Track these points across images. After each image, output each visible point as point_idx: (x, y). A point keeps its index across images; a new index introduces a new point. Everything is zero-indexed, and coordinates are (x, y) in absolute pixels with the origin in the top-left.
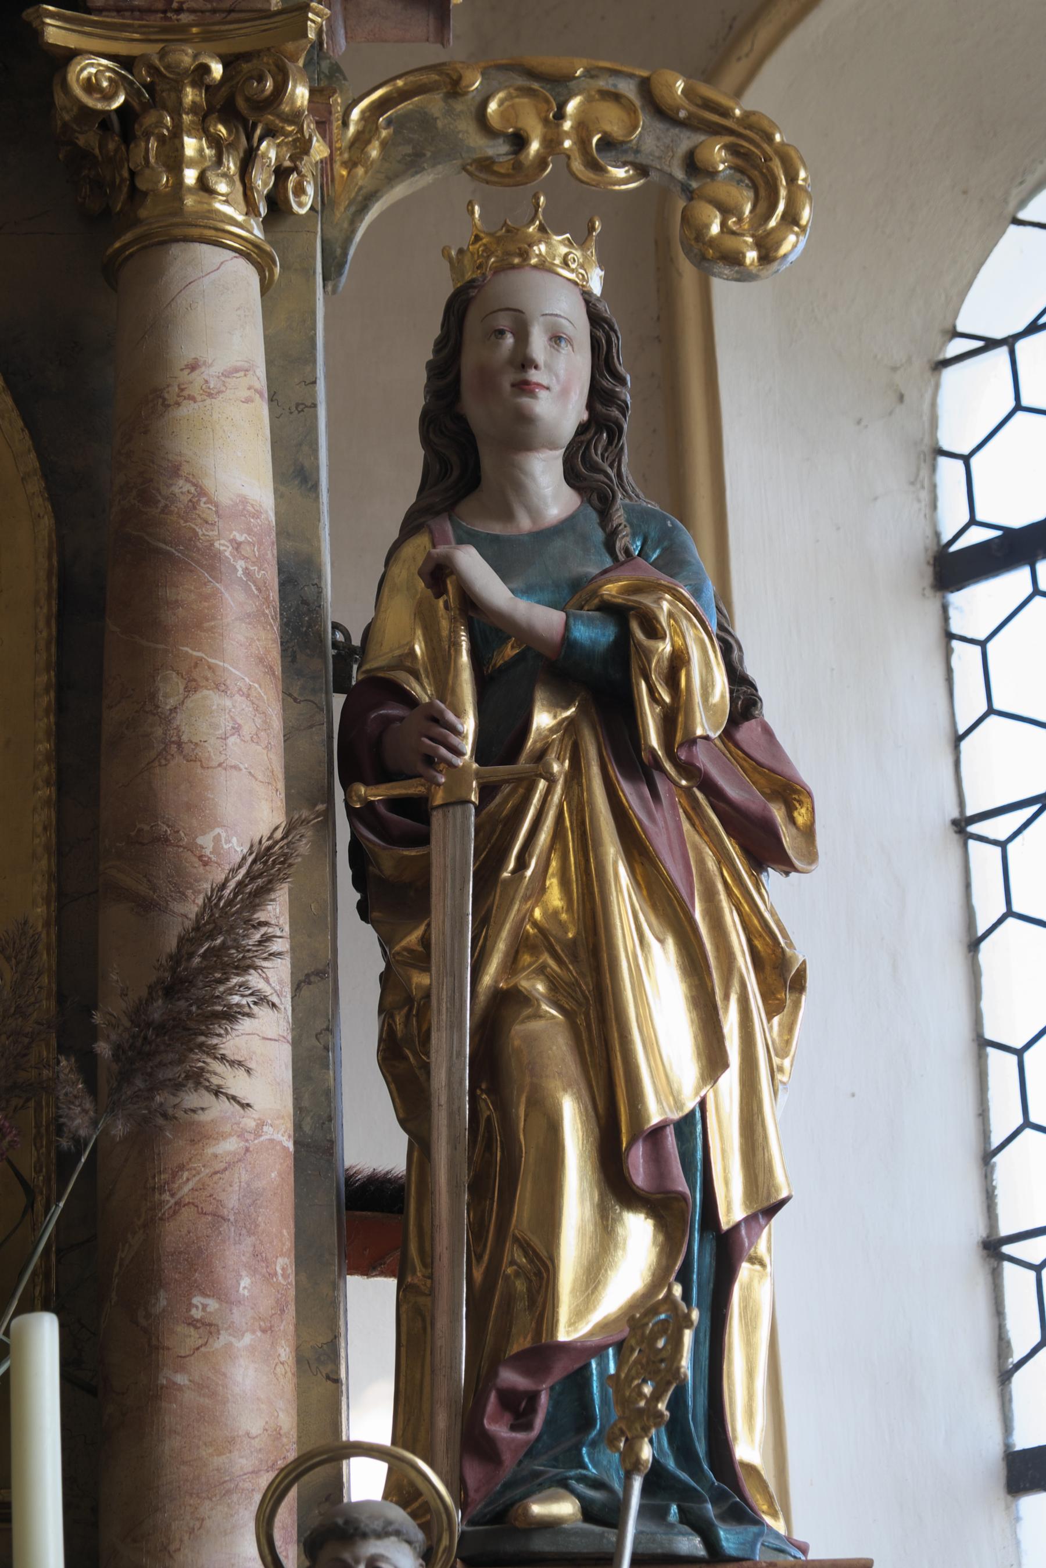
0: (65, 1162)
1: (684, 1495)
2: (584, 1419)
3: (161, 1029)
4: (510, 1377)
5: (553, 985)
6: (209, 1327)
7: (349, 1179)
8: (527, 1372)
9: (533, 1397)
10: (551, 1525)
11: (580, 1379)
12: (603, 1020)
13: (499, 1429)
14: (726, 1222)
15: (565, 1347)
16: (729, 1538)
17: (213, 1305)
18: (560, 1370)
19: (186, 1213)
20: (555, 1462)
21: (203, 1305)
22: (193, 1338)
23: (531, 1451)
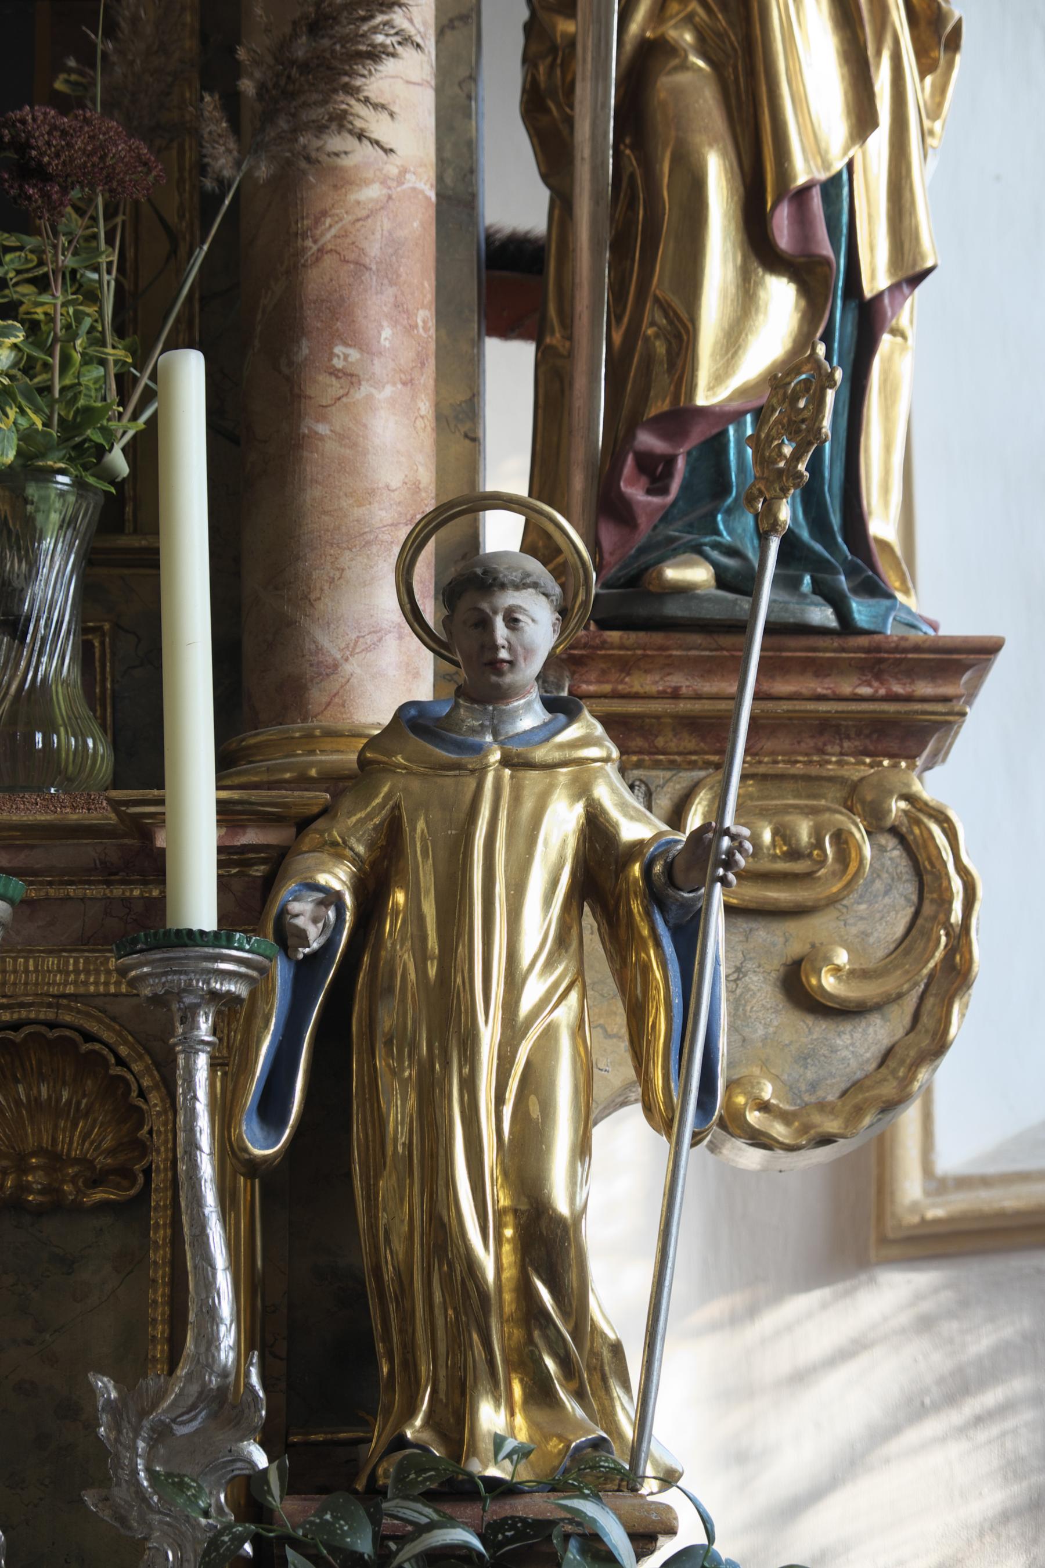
0: (209, 203)
1: (818, 566)
2: (721, 487)
3: (305, 67)
4: (647, 440)
5: (701, 38)
6: (350, 378)
7: (489, 237)
8: (666, 435)
9: (670, 461)
10: (684, 590)
11: (717, 445)
12: (751, 73)
13: (635, 492)
14: (869, 290)
15: (703, 411)
16: (861, 611)
17: (354, 355)
18: (698, 435)
19: (328, 260)
20: (690, 528)
21: (344, 355)
22: (335, 387)
23: (667, 516)
